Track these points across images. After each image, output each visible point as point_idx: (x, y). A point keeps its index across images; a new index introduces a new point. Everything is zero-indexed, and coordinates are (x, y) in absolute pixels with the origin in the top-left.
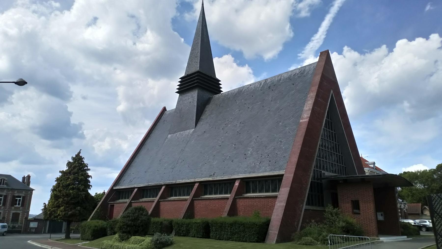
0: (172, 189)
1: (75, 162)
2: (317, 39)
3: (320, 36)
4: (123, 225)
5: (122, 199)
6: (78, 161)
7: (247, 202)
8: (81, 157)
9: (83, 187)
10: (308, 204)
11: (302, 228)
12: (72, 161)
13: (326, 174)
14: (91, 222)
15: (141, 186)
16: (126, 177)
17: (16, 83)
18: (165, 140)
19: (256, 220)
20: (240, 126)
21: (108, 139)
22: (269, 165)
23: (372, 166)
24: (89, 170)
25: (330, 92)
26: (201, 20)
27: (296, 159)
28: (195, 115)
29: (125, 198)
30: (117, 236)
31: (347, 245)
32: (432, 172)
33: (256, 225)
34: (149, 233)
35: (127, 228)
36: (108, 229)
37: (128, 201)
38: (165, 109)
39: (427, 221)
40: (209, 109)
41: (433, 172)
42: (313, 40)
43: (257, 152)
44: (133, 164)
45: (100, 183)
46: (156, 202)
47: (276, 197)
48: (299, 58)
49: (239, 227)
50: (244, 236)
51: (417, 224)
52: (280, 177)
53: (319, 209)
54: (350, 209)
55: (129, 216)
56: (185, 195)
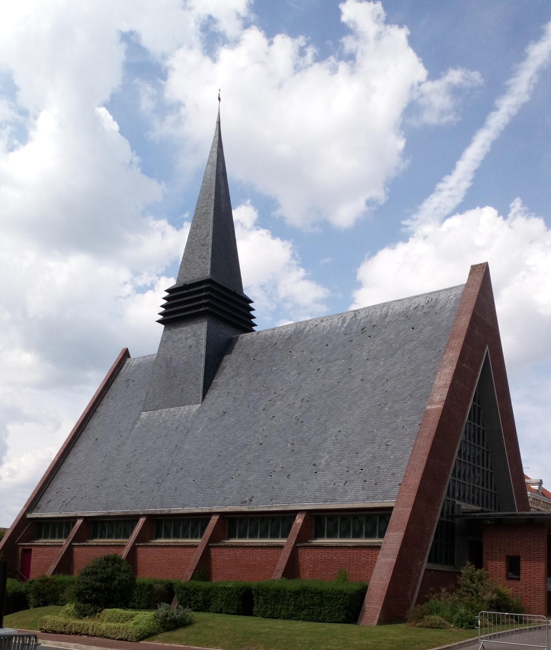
0: (160, 524)
2: (450, 189)
3: (459, 181)
4: (87, 589)
5: (46, 537)
7: (320, 554)
10: (429, 561)
11: (422, 600)
13: (463, 507)
15: (93, 515)
18: (135, 423)
19: (344, 587)
20: (301, 407)
22: (364, 488)
23: (536, 487)
25: (483, 350)
26: (215, 159)
27: (418, 481)
28: (202, 374)
29: (60, 537)
30: (70, 607)
31: (499, 630)
33: (345, 594)
34: (131, 604)
37: (65, 542)
38: (126, 354)
40: (230, 363)
42: (440, 190)
43: (340, 461)
44: (65, 468)
47: (378, 547)
48: (404, 230)
49: (312, 597)
50: (321, 612)
53: (446, 568)
54: (503, 571)
55: (96, 573)
56: (187, 537)
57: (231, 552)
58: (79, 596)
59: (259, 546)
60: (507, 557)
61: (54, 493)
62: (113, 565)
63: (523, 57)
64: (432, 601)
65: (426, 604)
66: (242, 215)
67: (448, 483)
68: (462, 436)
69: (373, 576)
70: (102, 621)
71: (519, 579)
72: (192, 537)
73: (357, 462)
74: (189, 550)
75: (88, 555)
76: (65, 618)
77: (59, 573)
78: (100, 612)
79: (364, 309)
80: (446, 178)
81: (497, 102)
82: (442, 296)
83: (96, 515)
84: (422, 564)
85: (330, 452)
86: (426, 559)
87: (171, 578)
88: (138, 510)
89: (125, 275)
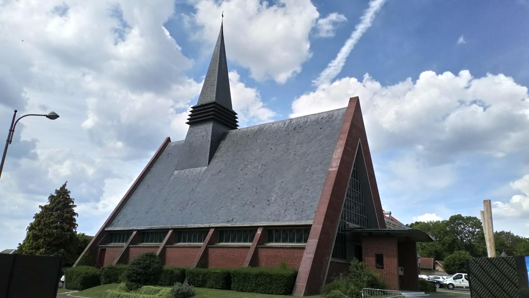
0: (180, 234)
1: (58, 196)
2: (335, 66)
3: (339, 63)
4: (134, 273)
5: (115, 242)
6: (63, 195)
7: (271, 252)
8: (67, 190)
9: (68, 226)
10: (333, 257)
11: (329, 281)
12: (56, 195)
13: (350, 225)
14: (78, 267)
16: (120, 217)
17: (47, 116)
18: (171, 177)
19: (285, 272)
20: (261, 169)
21: (68, 163)
23: (388, 216)
24: (75, 206)
25: (358, 141)
26: (220, 44)
27: (325, 210)
28: (209, 151)
29: (123, 242)
30: (123, 285)
32: (445, 223)
33: (285, 277)
34: (160, 282)
35: (137, 277)
36: (102, 277)
37: (125, 245)
38: (169, 140)
39: (441, 277)
40: (224, 145)
41: (446, 224)
42: (330, 67)
43: (282, 198)
44: (130, 202)
45: (89, 221)
46: (161, 247)
47: (303, 248)
48: (313, 85)
49: (266, 279)
51: (431, 280)
52: (308, 228)
55: (140, 264)
56: (196, 242)
57: (221, 250)
58: (129, 277)
59: (236, 247)
60: (376, 255)
61: (122, 216)
62: (150, 258)
63: (368, 7)
64: (335, 281)
65: (331, 283)
66: (232, 76)
67: (342, 211)
68: (348, 186)
69: (301, 266)
70: (141, 293)
71: (383, 268)
72: (198, 242)
73: (292, 199)
74: (197, 249)
75: (138, 252)
76: (120, 291)
77: (120, 263)
78: (140, 287)
79: (295, 118)
80: (333, 61)
81: (356, 27)
82: (335, 113)
83: (144, 229)
84: (329, 259)
85: (277, 193)
86: (331, 255)
87: (182, 266)
88: (169, 226)
89: (171, 102)
